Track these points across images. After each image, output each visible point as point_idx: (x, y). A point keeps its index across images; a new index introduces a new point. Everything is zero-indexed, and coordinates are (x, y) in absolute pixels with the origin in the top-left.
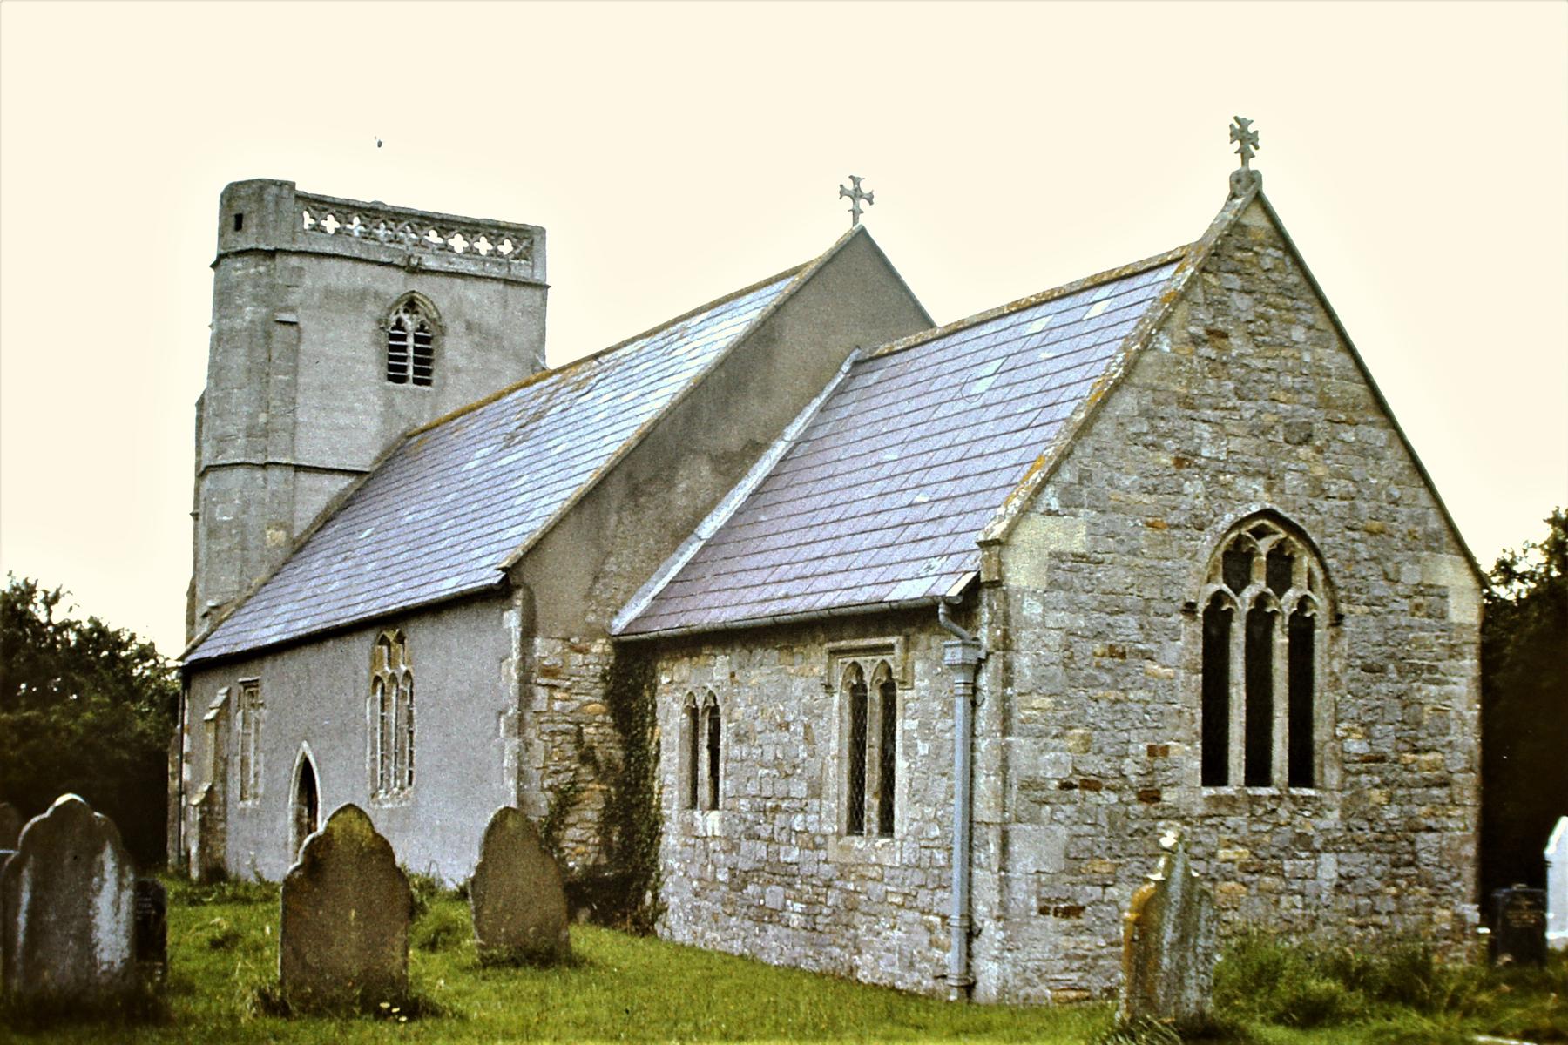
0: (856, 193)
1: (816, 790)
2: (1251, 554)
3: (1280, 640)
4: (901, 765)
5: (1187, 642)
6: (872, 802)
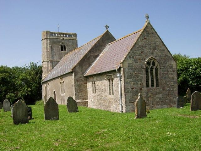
0: (107, 27)
1: (105, 91)
2: (150, 62)
3: (154, 71)
4: (114, 87)
5: (144, 71)
6: (111, 91)
